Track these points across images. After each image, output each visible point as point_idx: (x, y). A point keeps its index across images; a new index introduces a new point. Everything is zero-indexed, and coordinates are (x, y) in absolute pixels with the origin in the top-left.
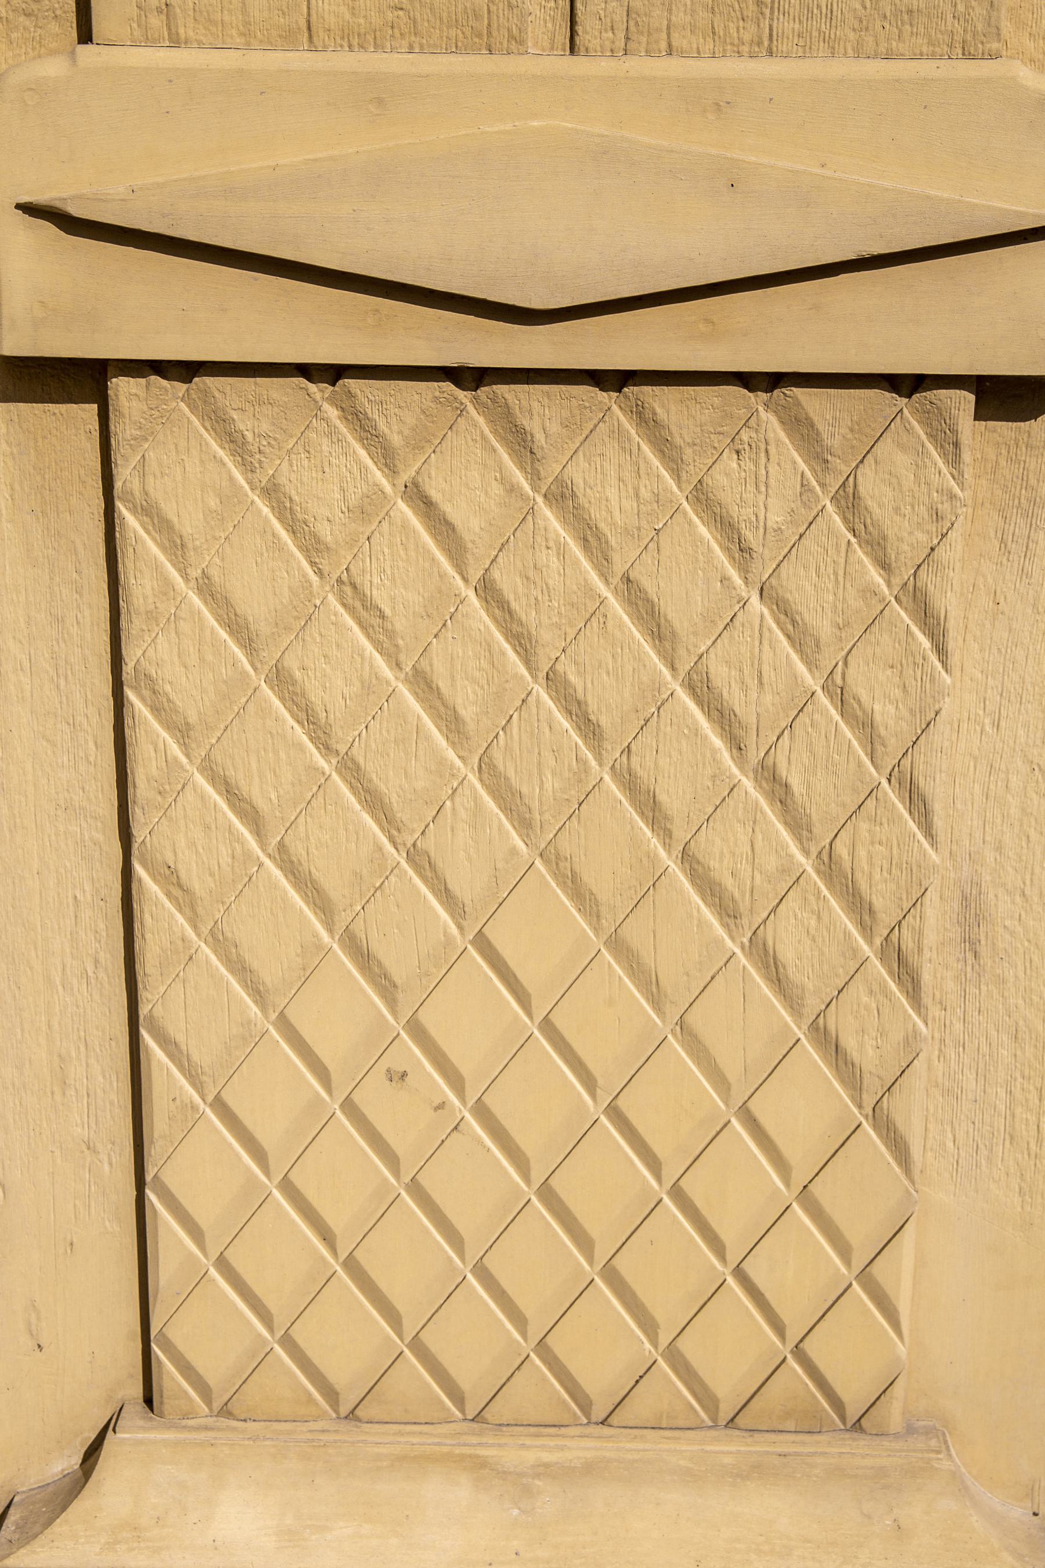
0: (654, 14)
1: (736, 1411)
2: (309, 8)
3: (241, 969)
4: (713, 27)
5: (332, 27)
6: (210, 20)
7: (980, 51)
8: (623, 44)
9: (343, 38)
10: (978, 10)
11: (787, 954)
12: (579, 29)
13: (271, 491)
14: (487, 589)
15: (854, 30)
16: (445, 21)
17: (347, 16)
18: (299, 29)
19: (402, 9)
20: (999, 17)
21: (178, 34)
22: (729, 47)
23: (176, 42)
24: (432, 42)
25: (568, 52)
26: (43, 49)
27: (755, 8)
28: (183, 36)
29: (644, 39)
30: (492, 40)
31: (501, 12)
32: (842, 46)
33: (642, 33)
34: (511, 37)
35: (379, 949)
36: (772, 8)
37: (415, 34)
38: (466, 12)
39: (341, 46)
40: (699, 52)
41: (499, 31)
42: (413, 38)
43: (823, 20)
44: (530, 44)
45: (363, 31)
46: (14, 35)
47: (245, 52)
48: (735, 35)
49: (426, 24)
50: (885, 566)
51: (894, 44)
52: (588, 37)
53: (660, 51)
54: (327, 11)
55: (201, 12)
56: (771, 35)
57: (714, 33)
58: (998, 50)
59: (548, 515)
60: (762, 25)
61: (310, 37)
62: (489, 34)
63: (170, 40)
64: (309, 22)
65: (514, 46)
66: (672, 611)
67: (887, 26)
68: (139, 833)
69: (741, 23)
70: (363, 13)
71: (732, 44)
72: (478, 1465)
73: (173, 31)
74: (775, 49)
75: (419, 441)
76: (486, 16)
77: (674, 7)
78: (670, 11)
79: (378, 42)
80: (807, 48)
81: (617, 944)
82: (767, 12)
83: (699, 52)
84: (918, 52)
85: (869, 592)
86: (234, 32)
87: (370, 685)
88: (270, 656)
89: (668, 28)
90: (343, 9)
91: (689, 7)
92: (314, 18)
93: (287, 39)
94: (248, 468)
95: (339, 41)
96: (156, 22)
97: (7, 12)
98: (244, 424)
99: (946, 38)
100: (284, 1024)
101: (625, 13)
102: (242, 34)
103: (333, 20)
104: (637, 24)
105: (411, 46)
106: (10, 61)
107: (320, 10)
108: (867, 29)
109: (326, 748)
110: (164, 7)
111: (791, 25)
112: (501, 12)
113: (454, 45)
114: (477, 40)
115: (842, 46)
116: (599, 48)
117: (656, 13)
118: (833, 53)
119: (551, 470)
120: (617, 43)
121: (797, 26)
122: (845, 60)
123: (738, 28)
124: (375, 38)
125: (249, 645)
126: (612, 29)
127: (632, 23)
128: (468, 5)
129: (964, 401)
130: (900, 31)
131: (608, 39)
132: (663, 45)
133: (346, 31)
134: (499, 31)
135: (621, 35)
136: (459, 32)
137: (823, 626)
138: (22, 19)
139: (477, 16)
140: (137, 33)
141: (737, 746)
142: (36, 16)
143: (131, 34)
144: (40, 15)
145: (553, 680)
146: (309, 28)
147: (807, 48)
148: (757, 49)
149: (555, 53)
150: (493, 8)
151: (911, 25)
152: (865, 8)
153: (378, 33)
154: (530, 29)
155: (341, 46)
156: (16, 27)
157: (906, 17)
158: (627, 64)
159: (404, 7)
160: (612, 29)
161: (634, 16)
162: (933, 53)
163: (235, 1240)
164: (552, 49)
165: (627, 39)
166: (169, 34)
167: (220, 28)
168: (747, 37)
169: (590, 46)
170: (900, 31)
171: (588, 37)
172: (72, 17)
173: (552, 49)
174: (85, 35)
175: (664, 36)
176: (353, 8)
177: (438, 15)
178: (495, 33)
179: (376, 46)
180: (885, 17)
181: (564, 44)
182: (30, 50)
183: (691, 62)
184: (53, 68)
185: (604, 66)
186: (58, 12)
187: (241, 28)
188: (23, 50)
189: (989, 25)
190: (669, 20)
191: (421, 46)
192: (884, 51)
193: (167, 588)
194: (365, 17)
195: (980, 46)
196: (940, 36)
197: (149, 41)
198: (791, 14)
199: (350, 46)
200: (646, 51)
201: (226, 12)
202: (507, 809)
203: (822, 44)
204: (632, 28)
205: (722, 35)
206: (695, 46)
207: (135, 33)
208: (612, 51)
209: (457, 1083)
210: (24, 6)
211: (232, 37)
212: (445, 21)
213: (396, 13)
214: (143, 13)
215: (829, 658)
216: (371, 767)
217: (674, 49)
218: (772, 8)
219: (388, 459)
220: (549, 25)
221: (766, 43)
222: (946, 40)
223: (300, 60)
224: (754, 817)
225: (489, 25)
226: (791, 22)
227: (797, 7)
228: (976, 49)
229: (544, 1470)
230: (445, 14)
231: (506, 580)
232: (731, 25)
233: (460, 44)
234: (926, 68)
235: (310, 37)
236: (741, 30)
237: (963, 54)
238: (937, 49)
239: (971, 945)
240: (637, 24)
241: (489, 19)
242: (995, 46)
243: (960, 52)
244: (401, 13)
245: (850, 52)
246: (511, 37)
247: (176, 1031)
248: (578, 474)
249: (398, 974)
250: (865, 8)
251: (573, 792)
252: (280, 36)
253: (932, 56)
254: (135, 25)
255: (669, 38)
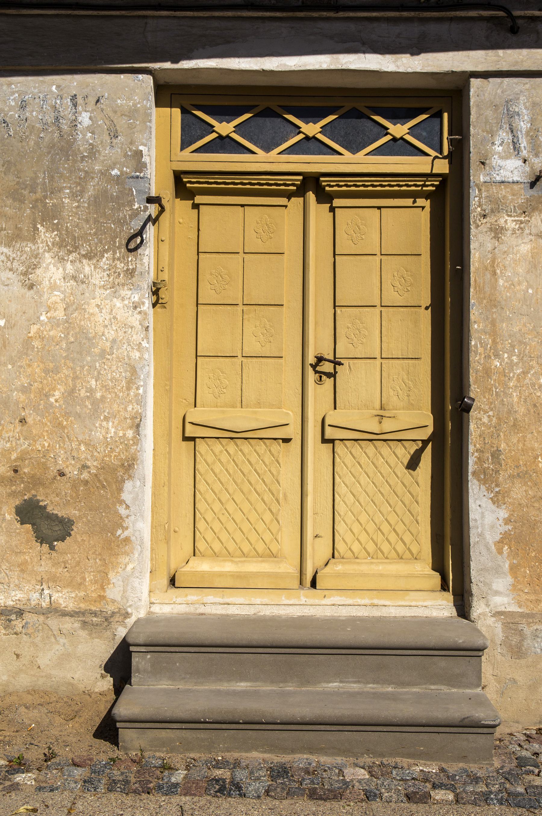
3: (206, 502)
11: (265, 499)
13: (211, 450)
14: (233, 460)
35: (221, 499)
50: (274, 457)
59: (240, 452)
66: (252, 462)
68: (196, 486)
72: (232, 561)
75: (227, 445)
81: (247, 499)
85: (272, 460)
87: (221, 470)
88: (211, 467)
93: (215, 407)
94: (209, 447)
98: (209, 443)
100: (211, 508)
109: (216, 477)
119: (240, 448)
125: (209, 466)
129: (281, 441)
137: (268, 463)
141: (259, 477)
145: (240, 470)
163: (255, 360)
184: (192, 410)
193: (200, 460)
202: (235, 484)
209: (230, 515)
215: (269, 467)
216: (221, 479)
219: (223, 447)
223: (216, 409)
224: (261, 484)
229: (239, 561)
231: (235, 459)
234: (275, 410)
239: (285, 499)
247: (199, 509)
248: (242, 448)
249: (224, 502)
251: (492, 796)
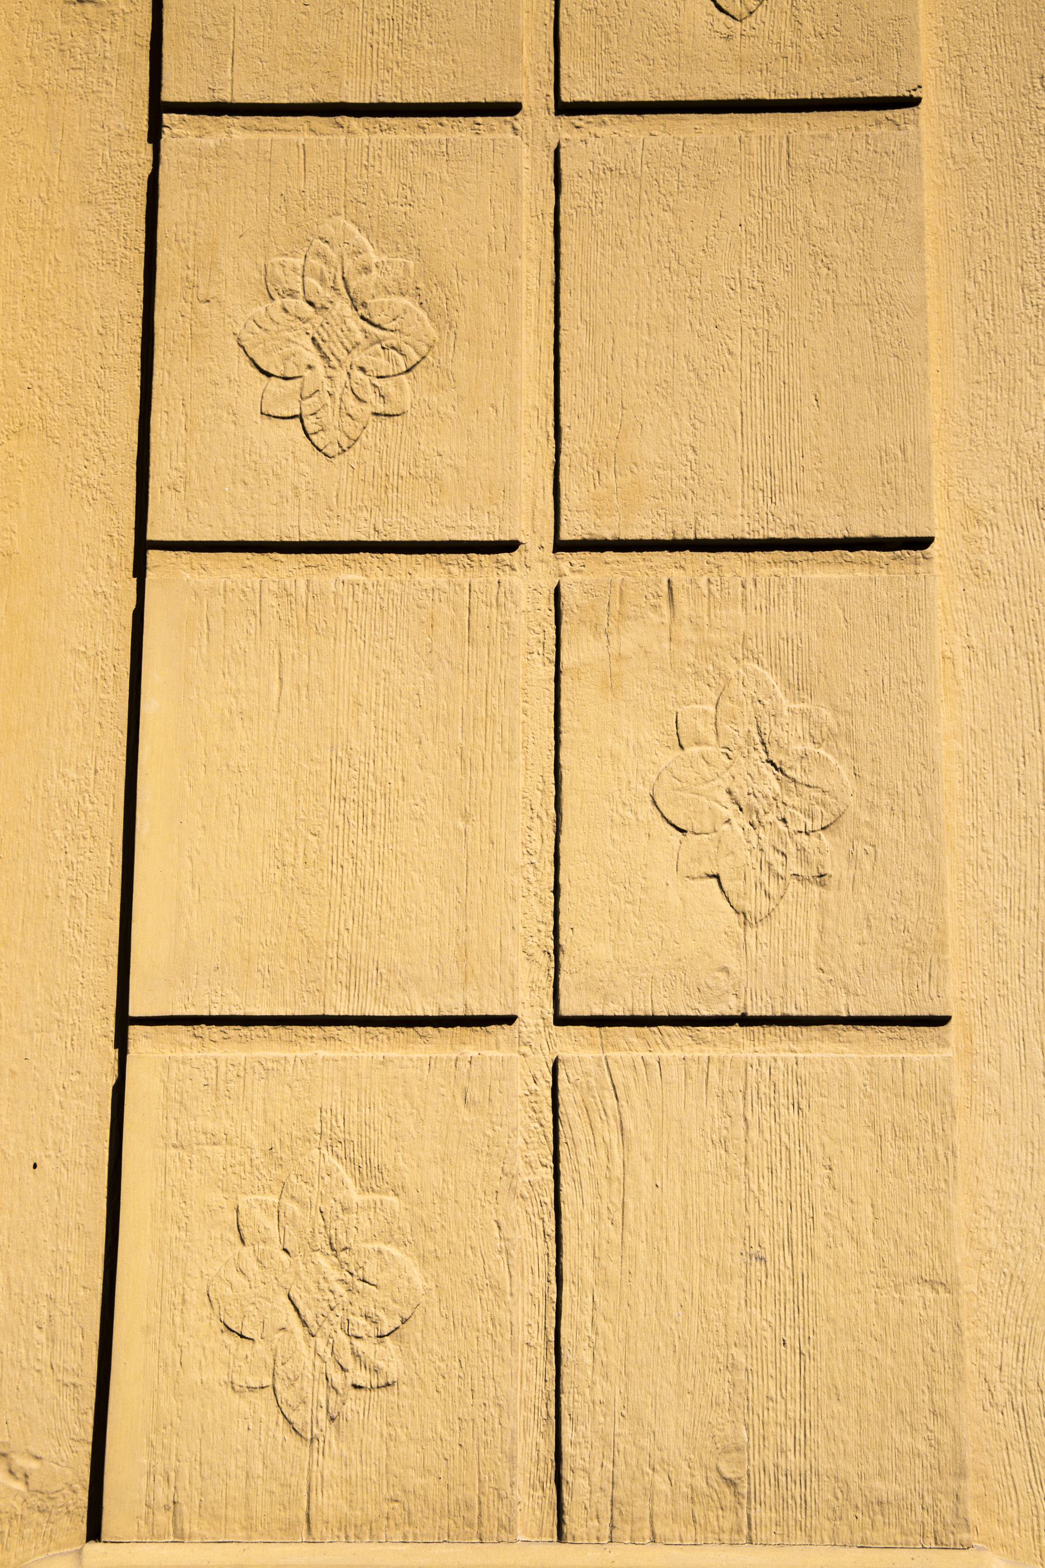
0: (637, 1504)
1: (905, 1031)
2: (309, 1502)
4: (693, 1516)
5: (331, 1519)
6: (214, 1516)
7: (952, 1541)
8: (608, 1533)
9: (340, 1529)
10: (945, 1503)
12: (566, 1518)
15: (828, 1519)
16: (438, 1511)
17: (346, 1509)
18: (299, 1521)
19: (397, 1501)
20: (966, 1510)
21: (182, 1530)
22: (710, 1535)
23: (180, 1537)
24: (425, 1532)
25: (555, 1539)
26: (52, 1544)
27: (733, 1498)
28: (187, 1532)
29: (628, 1528)
30: (483, 1529)
31: (491, 1502)
32: (818, 1533)
33: (626, 1522)
34: (501, 1526)
36: (749, 1498)
37: (409, 1524)
38: (458, 1504)
39: (338, 1537)
40: (681, 1540)
41: (489, 1520)
42: (407, 1528)
43: (798, 1510)
44: (519, 1531)
45: (359, 1523)
46: (27, 1531)
47: (246, 1546)
48: (715, 1523)
49: (420, 1515)
51: (868, 1532)
52: (574, 1525)
53: (644, 1539)
54: (325, 1504)
55: (206, 1509)
56: (749, 1524)
57: (695, 1522)
58: (969, 1541)
60: (740, 1514)
61: (309, 1529)
62: (480, 1523)
63: (175, 1535)
64: (308, 1515)
65: (504, 1536)
67: (859, 1515)
69: (720, 1512)
70: (360, 1506)
71: (713, 1532)
73: (179, 1526)
74: (754, 1537)
76: (477, 1506)
77: (655, 1498)
78: (651, 1500)
79: (374, 1533)
80: (785, 1536)
82: (745, 1502)
83: (681, 1540)
84: (892, 1541)
86: (236, 1526)
89: (651, 1516)
90: (341, 1502)
91: (669, 1497)
92: (313, 1512)
95: (336, 1532)
96: (163, 1519)
97: (22, 1509)
99: (917, 1528)
101: (609, 1503)
102: (244, 1528)
103: (331, 1512)
104: (621, 1513)
105: (405, 1536)
106: (20, 1557)
107: (320, 1504)
108: (841, 1519)
110: (171, 1505)
111: (769, 1514)
112: (491, 1502)
113: (446, 1535)
114: (467, 1529)
115: (818, 1533)
116: (585, 1536)
117: (639, 1502)
118: (810, 1541)
120: (603, 1531)
121: (774, 1515)
122: (822, 1549)
123: (718, 1517)
124: (371, 1529)
126: (598, 1517)
127: (616, 1512)
128: (460, 1497)
130: (873, 1521)
131: (594, 1527)
132: (647, 1533)
133: (343, 1524)
134: (489, 1520)
135: (606, 1523)
136: (451, 1522)
138: (36, 1515)
139: (468, 1507)
140: (144, 1530)
142: (50, 1513)
143: (138, 1531)
144: (54, 1511)
146: (308, 1521)
147: (785, 1536)
148: (737, 1537)
149: (544, 1539)
150: (483, 1499)
151: (883, 1515)
152: (837, 1499)
153: (374, 1524)
154: (519, 1517)
155: (338, 1537)
156: (29, 1523)
157: (877, 1508)
158: (612, 1554)
159: (399, 1499)
160: (598, 1517)
161: (618, 1505)
162: (907, 1543)
164: (541, 1535)
165: (612, 1527)
166: (174, 1531)
167: (223, 1523)
168: (726, 1525)
169: (577, 1534)
170: (873, 1521)
171: (574, 1525)
172: (84, 1512)
173: (541, 1535)
174: (94, 1533)
175: (648, 1524)
176: (351, 1501)
177: (431, 1507)
178: (485, 1522)
179: (371, 1536)
180: (857, 1507)
181: (552, 1531)
182: (40, 1545)
183: (674, 1551)
185: (591, 1554)
186: (71, 1508)
187: (244, 1522)
188: (34, 1546)
189: (957, 1516)
190: (651, 1510)
191: (415, 1535)
192: (859, 1540)
194: (362, 1509)
195: (951, 1536)
196: (911, 1526)
197: (154, 1538)
198: (768, 1505)
199: (347, 1537)
200: (631, 1539)
201: (229, 1508)
203: (799, 1532)
204: (616, 1516)
205: (702, 1522)
206: (677, 1534)
207: (142, 1530)
208: (598, 1538)
210: (39, 1503)
211: (234, 1531)
212: (438, 1511)
213: (391, 1505)
214: (151, 1511)
217: (658, 1537)
218: (749, 1498)
220: (538, 1513)
221: (745, 1531)
222: (918, 1531)
225: (480, 1515)
226: (768, 1511)
227: (773, 1497)
228: (947, 1538)
230: (438, 1506)
232: (711, 1514)
233: (452, 1533)
235: (309, 1529)
236: (721, 1518)
237: (936, 1544)
238: (910, 1539)
240: (621, 1513)
241: (480, 1509)
242: (965, 1536)
243: (933, 1541)
244: (396, 1505)
245: (827, 1541)
246: (501, 1526)
250: (837, 1499)
252: (280, 1529)
253: (906, 1546)
254: (142, 1523)
255: (652, 1526)
